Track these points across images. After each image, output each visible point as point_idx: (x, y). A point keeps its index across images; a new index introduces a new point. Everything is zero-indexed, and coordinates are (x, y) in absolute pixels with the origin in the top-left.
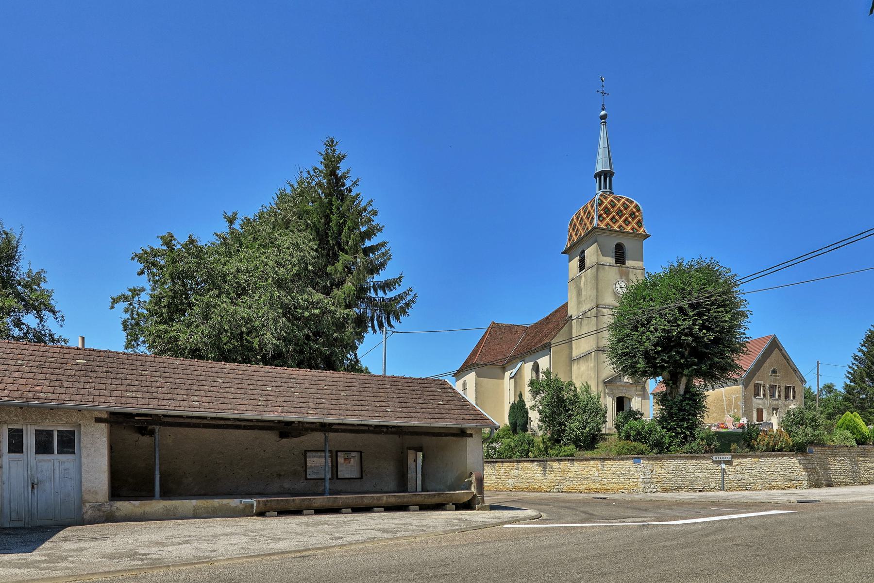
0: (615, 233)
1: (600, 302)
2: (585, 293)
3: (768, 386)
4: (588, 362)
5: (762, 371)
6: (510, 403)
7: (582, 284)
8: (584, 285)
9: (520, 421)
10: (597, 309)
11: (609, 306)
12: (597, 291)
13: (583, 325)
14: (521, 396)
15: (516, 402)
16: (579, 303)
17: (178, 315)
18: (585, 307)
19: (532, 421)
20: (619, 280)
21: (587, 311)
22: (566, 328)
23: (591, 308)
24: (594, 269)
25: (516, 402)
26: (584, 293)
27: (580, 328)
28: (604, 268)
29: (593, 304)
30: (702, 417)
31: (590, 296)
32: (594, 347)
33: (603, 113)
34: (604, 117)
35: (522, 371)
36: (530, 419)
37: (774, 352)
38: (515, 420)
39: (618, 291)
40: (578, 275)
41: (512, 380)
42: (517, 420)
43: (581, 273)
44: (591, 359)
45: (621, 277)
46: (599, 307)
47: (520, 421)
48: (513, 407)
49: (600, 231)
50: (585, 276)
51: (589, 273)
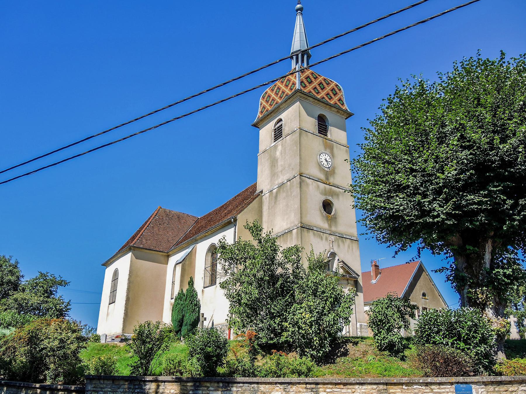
0: (318, 102)
1: (303, 171)
2: (282, 163)
3: (421, 307)
4: (287, 244)
5: (415, 292)
6: (172, 299)
7: (278, 153)
8: (281, 154)
9: (189, 318)
10: (300, 178)
11: (313, 177)
12: (300, 158)
13: (278, 199)
14: (191, 283)
15: (185, 291)
16: (273, 175)
17: (16, 311)
18: (282, 178)
19: (205, 319)
20: (323, 151)
21: (286, 181)
22: (255, 203)
23: (292, 177)
24: (297, 134)
25: (185, 291)
26: (280, 163)
27: (275, 203)
28: (307, 135)
29: (296, 172)
30: (117, 371)
31: (290, 165)
32: (297, 223)
33: (299, 6)
34: (301, 9)
35: (193, 257)
36: (203, 317)
37: (423, 274)
38: (180, 317)
39: (322, 163)
40: (272, 145)
41: (179, 268)
42: (183, 316)
43: (277, 142)
44: (292, 239)
45: (326, 148)
46: (303, 176)
47: (189, 318)
48: (181, 297)
49: (303, 95)
50: (282, 145)
51: (287, 140)
